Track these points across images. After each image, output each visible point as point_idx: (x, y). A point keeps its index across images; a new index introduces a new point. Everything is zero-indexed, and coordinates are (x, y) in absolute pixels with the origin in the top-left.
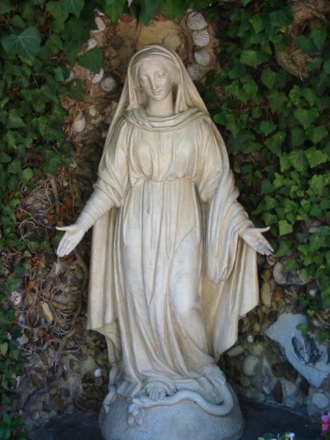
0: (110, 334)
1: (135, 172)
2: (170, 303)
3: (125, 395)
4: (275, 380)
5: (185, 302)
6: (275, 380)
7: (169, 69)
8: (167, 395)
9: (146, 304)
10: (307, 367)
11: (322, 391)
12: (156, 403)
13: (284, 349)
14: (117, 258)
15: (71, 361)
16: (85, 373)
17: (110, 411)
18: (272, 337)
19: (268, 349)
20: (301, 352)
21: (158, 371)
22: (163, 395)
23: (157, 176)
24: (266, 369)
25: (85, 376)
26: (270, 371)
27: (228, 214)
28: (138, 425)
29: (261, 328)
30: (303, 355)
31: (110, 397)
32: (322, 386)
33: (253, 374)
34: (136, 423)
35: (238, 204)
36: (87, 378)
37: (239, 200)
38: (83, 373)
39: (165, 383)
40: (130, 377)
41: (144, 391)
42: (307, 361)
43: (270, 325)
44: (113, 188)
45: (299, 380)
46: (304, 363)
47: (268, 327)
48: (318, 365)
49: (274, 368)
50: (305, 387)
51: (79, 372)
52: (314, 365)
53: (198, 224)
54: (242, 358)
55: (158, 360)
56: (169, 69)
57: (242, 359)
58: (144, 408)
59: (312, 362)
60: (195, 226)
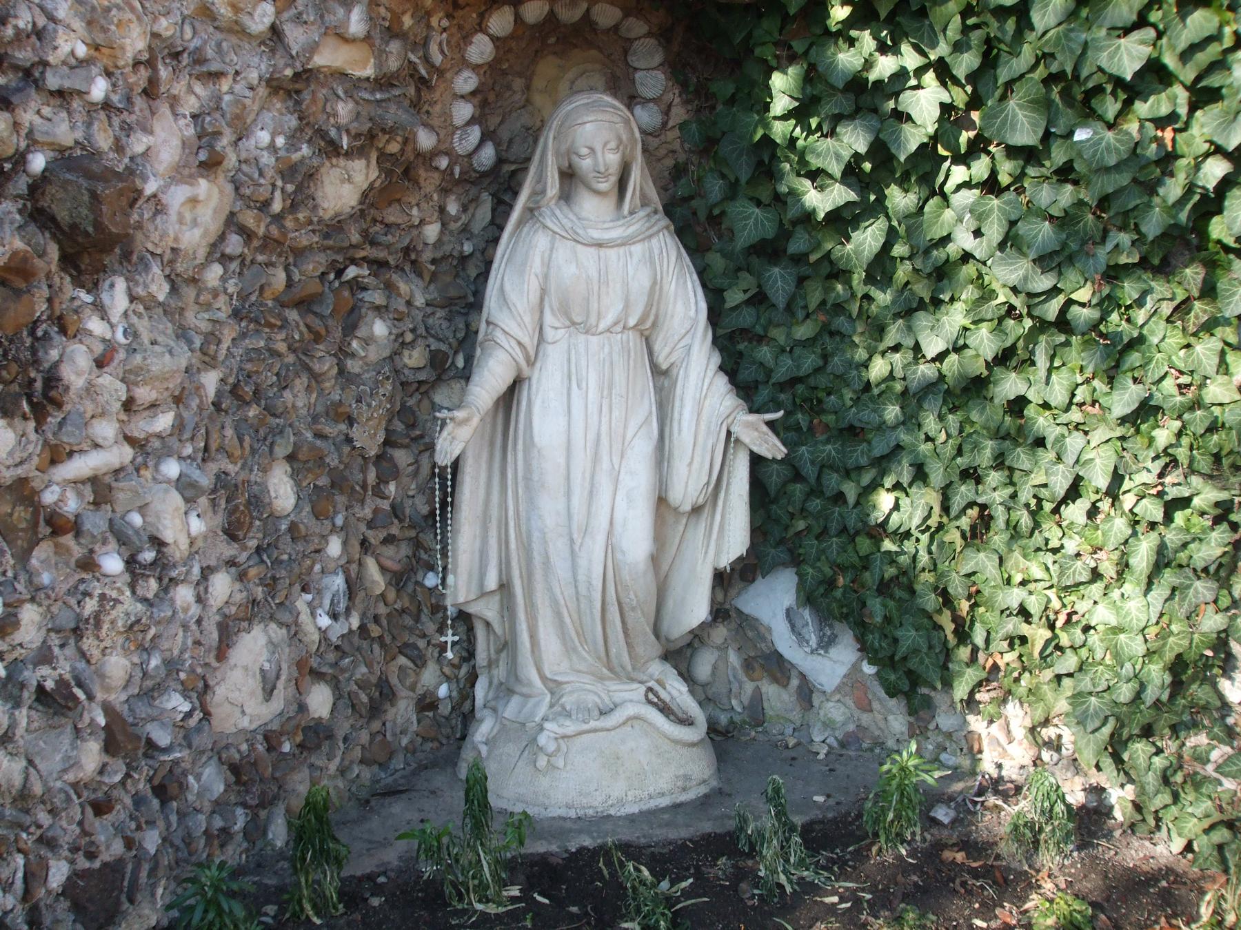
0: (488, 610)
1: (625, 284)
2: (610, 546)
3: (521, 719)
4: (749, 687)
5: (636, 541)
6: (749, 687)
7: (624, 137)
8: (602, 713)
9: (572, 552)
10: (815, 657)
11: (838, 697)
12: (585, 727)
13: (769, 629)
14: (516, 469)
15: (401, 669)
16: (421, 692)
17: (489, 752)
18: (746, 610)
19: (737, 632)
20: (804, 631)
21: (579, 671)
22: (596, 713)
23: (594, 324)
24: (734, 669)
25: (424, 696)
26: (740, 673)
27: (704, 392)
28: (555, 768)
29: (725, 595)
30: (807, 637)
31: (484, 730)
32: (838, 689)
33: (710, 679)
34: (552, 767)
35: (721, 373)
36: (428, 700)
37: (721, 368)
38: (420, 690)
39: (596, 693)
40: (530, 684)
41: (557, 708)
42: (814, 646)
43: (745, 588)
44: (519, 343)
45: (795, 682)
46: (808, 649)
47: (739, 594)
48: (833, 652)
49: (748, 665)
50: (806, 692)
51: (412, 688)
52: (826, 652)
53: (654, 409)
54: (689, 652)
55: (580, 649)
56: (624, 137)
57: (688, 654)
58: (564, 737)
59: (822, 648)
60: (651, 413)
